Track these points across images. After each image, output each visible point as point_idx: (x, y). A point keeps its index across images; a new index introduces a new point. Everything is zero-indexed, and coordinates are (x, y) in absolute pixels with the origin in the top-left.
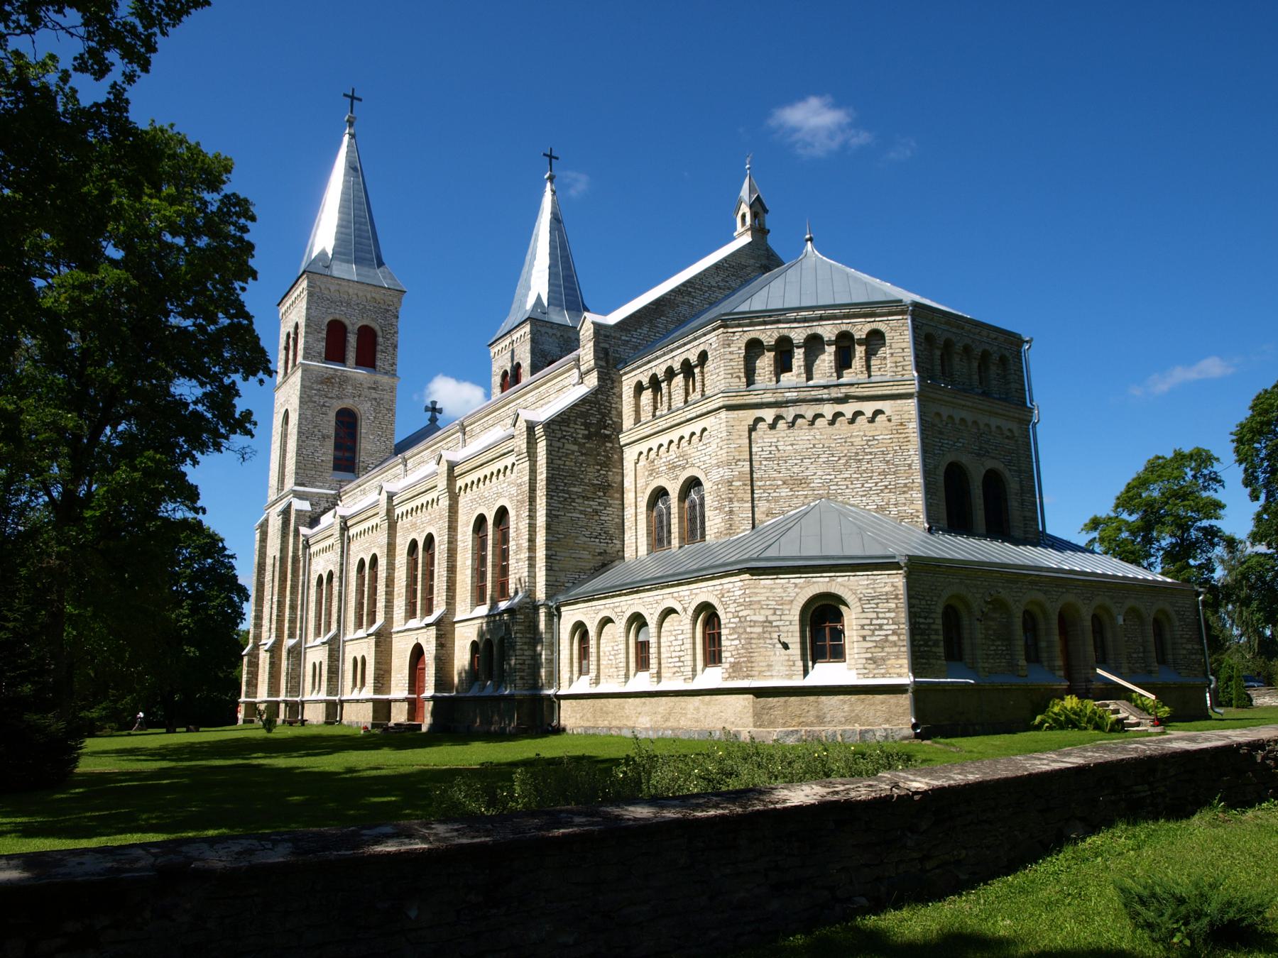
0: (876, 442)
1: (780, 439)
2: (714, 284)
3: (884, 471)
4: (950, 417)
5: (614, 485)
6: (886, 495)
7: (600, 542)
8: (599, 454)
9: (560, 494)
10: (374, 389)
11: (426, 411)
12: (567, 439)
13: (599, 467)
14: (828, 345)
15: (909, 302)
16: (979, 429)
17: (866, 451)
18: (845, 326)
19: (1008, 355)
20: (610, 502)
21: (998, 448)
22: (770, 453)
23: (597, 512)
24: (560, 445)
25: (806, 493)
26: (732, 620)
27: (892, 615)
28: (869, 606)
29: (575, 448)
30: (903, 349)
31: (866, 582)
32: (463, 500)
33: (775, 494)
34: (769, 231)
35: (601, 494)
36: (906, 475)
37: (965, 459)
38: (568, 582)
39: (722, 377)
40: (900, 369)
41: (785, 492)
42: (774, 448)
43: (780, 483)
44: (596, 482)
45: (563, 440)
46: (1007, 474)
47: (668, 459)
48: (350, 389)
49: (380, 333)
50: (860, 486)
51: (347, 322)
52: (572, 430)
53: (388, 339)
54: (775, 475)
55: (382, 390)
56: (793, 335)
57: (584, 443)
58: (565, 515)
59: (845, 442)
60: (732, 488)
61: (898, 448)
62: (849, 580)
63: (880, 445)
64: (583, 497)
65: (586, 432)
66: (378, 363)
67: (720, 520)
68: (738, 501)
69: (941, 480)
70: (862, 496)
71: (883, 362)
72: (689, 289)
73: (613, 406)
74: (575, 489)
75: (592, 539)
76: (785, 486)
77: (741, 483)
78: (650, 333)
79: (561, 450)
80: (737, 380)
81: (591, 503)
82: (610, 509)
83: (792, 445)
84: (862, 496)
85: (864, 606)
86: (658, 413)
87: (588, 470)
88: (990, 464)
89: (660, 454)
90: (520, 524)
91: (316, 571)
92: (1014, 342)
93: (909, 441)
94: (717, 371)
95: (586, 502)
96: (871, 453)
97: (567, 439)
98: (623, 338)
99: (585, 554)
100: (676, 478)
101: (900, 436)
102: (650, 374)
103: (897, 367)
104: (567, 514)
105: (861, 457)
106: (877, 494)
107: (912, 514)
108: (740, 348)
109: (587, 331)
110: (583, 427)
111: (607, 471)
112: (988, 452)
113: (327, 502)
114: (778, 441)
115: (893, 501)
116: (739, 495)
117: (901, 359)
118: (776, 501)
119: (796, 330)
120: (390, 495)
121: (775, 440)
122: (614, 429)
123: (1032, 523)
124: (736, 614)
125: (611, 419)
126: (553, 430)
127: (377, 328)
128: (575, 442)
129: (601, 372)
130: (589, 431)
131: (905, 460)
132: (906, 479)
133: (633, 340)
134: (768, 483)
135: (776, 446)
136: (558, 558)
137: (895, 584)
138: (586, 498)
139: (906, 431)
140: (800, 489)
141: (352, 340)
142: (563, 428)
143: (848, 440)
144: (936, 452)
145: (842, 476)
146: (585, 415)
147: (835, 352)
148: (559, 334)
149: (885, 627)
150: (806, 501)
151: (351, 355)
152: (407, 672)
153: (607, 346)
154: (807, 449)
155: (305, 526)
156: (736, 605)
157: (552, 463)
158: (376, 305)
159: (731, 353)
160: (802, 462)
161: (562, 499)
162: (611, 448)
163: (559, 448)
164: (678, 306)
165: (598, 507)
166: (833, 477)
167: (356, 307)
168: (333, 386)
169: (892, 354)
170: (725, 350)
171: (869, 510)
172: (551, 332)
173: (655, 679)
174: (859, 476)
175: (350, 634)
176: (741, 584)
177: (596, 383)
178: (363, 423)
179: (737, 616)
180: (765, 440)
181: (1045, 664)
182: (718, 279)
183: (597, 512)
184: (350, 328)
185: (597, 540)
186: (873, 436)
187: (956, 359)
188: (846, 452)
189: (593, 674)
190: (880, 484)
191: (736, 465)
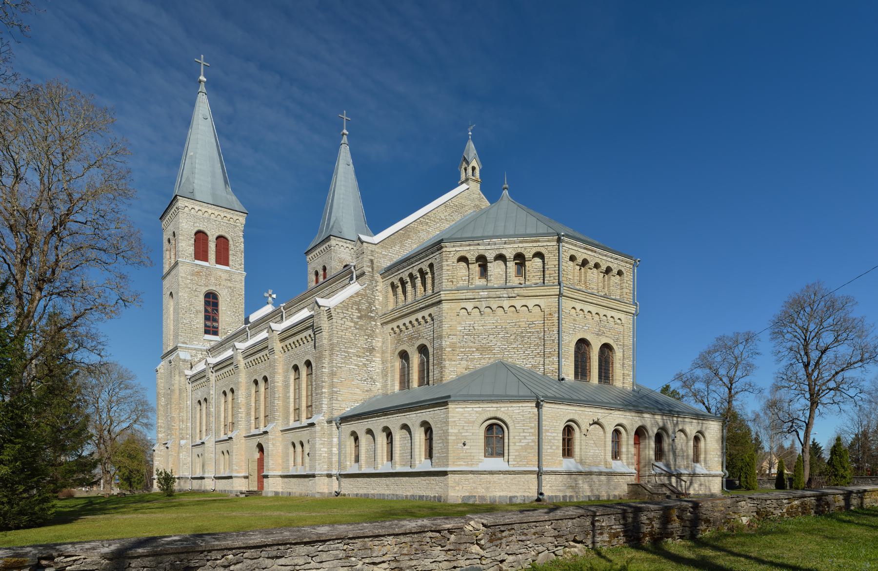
10: (229, 280)
12: (347, 319)
13: (367, 337)
22: (470, 331)
29: (352, 324)
31: (518, 411)
33: (471, 357)
42: (471, 328)
45: (343, 319)
49: (231, 242)
50: (522, 352)
51: (209, 233)
53: (237, 247)
56: (487, 254)
57: (358, 322)
59: (515, 325)
65: (359, 315)
66: (231, 263)
70: (524, 359)
72: (427, 221)
74: (352, 351)
77: (451, 349)
81: (362, 359)
83: (483, 326)
96: (530, 332)
97: (347, 319)
98: (383, 253)
110: (357, 311)
113: (202, 354)
116: (450, 357)
125: (375, 306)
126: (338, 313)
134: (467, 349)
135: (473, 327)
138: (360, 357)
142: (344, 312)
144: (571, 332)
145: (512, 346)
146: (358, 304)
153: (373, 258)
154: (492, 329)
163: (342, 324)
164: (419, 232)
165: (366, 362)
166: (507, 346)
172: (345, 245)
182: (446, 214)
186: (532, 322)
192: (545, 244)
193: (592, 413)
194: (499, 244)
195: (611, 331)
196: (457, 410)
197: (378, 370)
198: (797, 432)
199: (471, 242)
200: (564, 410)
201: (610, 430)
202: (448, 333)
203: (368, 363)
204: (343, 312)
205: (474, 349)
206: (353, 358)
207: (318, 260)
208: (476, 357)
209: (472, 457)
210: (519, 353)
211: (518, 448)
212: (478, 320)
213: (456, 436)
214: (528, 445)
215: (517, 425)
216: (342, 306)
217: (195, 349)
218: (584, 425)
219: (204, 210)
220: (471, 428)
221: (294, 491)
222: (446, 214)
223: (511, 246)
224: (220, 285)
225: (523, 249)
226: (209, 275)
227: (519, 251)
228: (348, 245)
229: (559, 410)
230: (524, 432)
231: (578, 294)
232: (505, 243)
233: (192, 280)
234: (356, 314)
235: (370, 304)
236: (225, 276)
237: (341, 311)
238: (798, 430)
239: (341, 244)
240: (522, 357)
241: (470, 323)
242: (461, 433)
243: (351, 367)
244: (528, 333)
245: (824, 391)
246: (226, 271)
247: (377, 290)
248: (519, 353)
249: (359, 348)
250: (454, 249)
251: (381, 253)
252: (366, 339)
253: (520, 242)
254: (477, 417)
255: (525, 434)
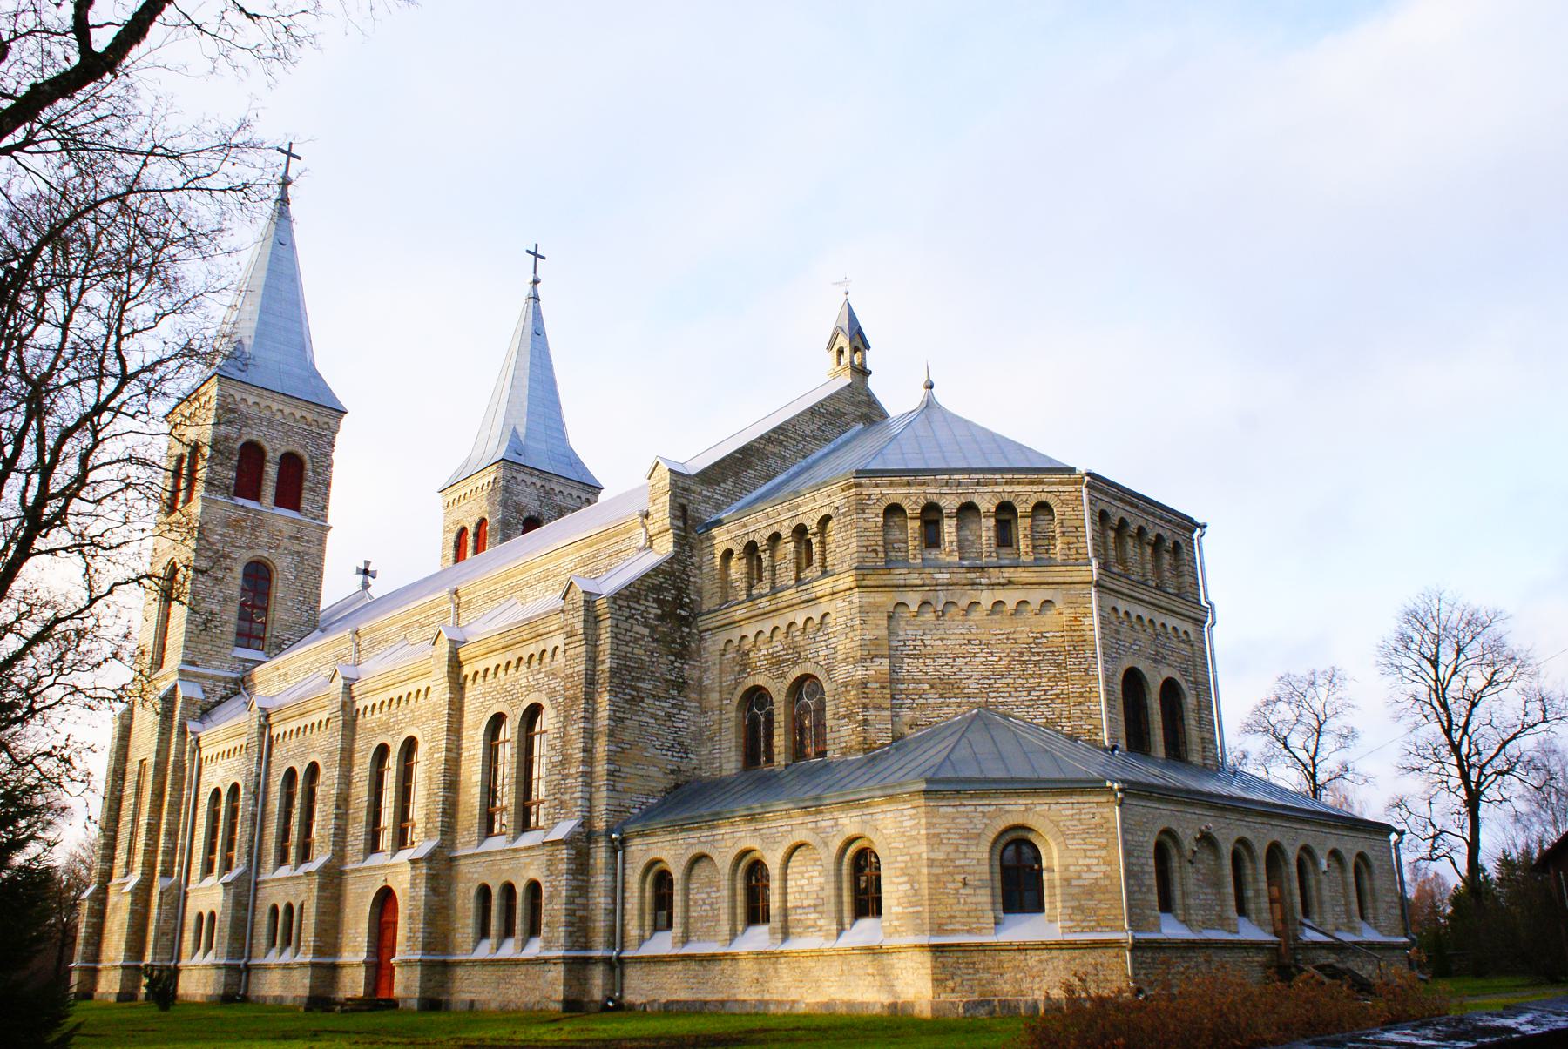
0: (1045, 640)
1: (927, 632)
2: (808, 432)
3: (1055, 677)
4: (1127, 613)
5: (690, 682)
6: (1057, 706)
7: (674, 756)
8: (674, 641)
9: (627, 691)
10: (297, 538)
11: (358, 573)
12: (637, 620)
13: (673, 658)
14: (985, 517)
15: (1083, 472)
16: (1155, 630)
17: (1033, 650)
18: (1006, 492)
19: (1181, 542)
20: (686, 703)
21: (1175, 654)
22: (915, 649)
23: (669, 716)
24: (627, 626)
25: (959, 700)
26: (899, 859)
27: (1104, 853)
28: (1075, 842)
29: (646, 631)
30: (1076, 528)
31: (1070, 812)
32: (472, 692)
33: (921, 701)
34: (871, 373)
35: (675, 693)
36: (1082, 682)
37: (1143, 666)
38: (634, 807)
39: (855, 550)
40: (1073, 551)
41: (933, 698)
42: (919, 643)
43: (926, 686)
44: (669, 677)
45: (630, 621)
46: (1184, 685)
47: (771, 651)
48: (264, 537)
49: (308, 465)
50: (1025, 694)
51: (267, 447)
52: (643, 608)
53: (319, 474)
54: (921, 676)
55: (308, 542)
56: (943, 503)
57: (657, 626)
58: (631, 719)
59: (1008, 639)
60: (866, 691)
61: (1072, 648)
62: (1049, 809)
63: (1050, 644)
64: (654, 696)
65: (659, 612)
66: (304, 505)
67: (850, 732)
68: (874, 708)
69: (1118, 689)
70: (1028, 706)
71: (1052, 542)
72: (781, 437)
73: (691, 579)
74: (644, 686)
75: (664, 752)
76: (933, 691)
77: (878, 685)
78: (736, 489)
79: (629, 634)
80: (874, 555)
81: (663, 704)
82: (685, 713)
83: (942, 640)
84: (1028, 706)
85: (1068, 842)
86: (755, 592)
87: (661, 660)
88: (1167, 672)
89: (758, 644)
90: (569, 728)
91: (209, 784)
92: (1189, 525)
93: (1085, 641)
94: (847, 542)
95: (657, 703)
96: (1038, 654)
97: (637, 620)
98: (705, 493)
99: (654, 771)
100: (783, 675)
101: (1075, 634)
102: (746, 540)
103: (1069, 549)
104: (634, 718)
105: (1027, 658)
106: (1047, 704)
107: (1089, 730)
108: (877, 515)
109: (660, 481)
110: (655, 605)
111: (682, 664)
112: (1165, 658)
113: (225, 688)
114: (924, 634)
115: (1065, 714)
116: (876, 701)
117: (1075, 540)
118: (921, 710)
119: (947, 497)
120: (347, 682)
121: (920, 632)
122: (692, 609)
123: (1211, 746)
124: (906, 850)
125: (688, 597)
126: (620, 607)
127: (306, 457)
128: (646, 624)
129: (678, 535)
130: (663, 611)
131: (1081, 663)
132: (1083, 687)
133: (716, 496)
134: (911, 686)
135: (922, 641)
136: (623, 775)
137: (1105, 815)
138: (659, 698)
139: (1081, 628)
140: (951, 695)
141: (272, 471)
142: (632, 604)
143: (1011, 636)
144: (1114, 655)
145: (1004, 681)
146: (658, 589)
147: (996, 526)
148: (539, 484)
149: (1095, 869)
150: (960, 711)
151: (269, 491)
152: (366, 926)
153: (685, 501)
154: (961, 645)
155: (194, 720)
156: (905, 839)
157: (617, 649)
158: (306, 427)
159: (866, 520)
160: (954, 661)
161: (628, 697)
162: (689, 633)
163: (626, 630)
164: (768, 458)
165: (671, 710)
166: (992, 681)
167: (280, 428)
168: (243, 532)
169: (1063, 533)
170: (860, 516)
171: (1037, 724)
172: (529, 480)
173: (779, 936)
174: (1025, 681)
175: (268, 874)
176: (914, 811)
177: (671, 549)
178: (280, 584)
179: (908, 854)
180: (908, 632)
181: (1253, 916)
182: (814, 427)
183: (669, 716)
184: (269, 455)
185: (670, 753)
186: (1041, 633)
187: (1130, 543)
188: (1008, 650)
189: (677, 929)
190: (1049, 693)
191: (872, 662)
192: (1054, 488)
193: (1196, 816)
194: (967, 484)
195: (1175, 654)
196: (942, 810)
197: (693, 728)
198: (1450, 858)
199: (911, 479)
200: (1153, 811)
201: (1227, 849)
202: (872, 652)
203: (675, 711)
204: (629, 607)
205: (927, 686)
206: (646, 700)
207: (469, 505)
208: (929, 701)
209: (980, 914)
210: (1018, 694)
211: (1076, 891)
212: (933, 627)
213: (942, 866)
214: (1096, 884)
215: (1071, 842)
216: (628, 593)
217: (211, 677)
218: (1189, 844)
219: (263, 403)
220: (973, 848)
221: (483, 997)
222: (814, 427)
223: (990, 488)
224: (277, 547)
225: (1013, 495)
226: (257, 526)
227: (1006, 498)
228: (534, 480)
229: (1145, 810)
230: (1086, 857)
231: (1119, 583)
232: (978, 483)
233: (223, 535)
234: (655, 611)
235: (680, 591)
236: (288, 530)
237: (625, 603)
238: (1453, 854)
239: (520, 477)
240: (1026, 703)
241: (914, 633)
242: (952, 861)
243: (644, 719)
244: (1033, 654)
245: (1487, 777)
246: (293, 521)
247: (693, 564)
248: (1018, 694)
249: (657, 680)
250: (877, 490)
251: (700, 494)
252: (672, 663)
253: (1006, 483)
254: (986, 825)
255: (1088, 861)
